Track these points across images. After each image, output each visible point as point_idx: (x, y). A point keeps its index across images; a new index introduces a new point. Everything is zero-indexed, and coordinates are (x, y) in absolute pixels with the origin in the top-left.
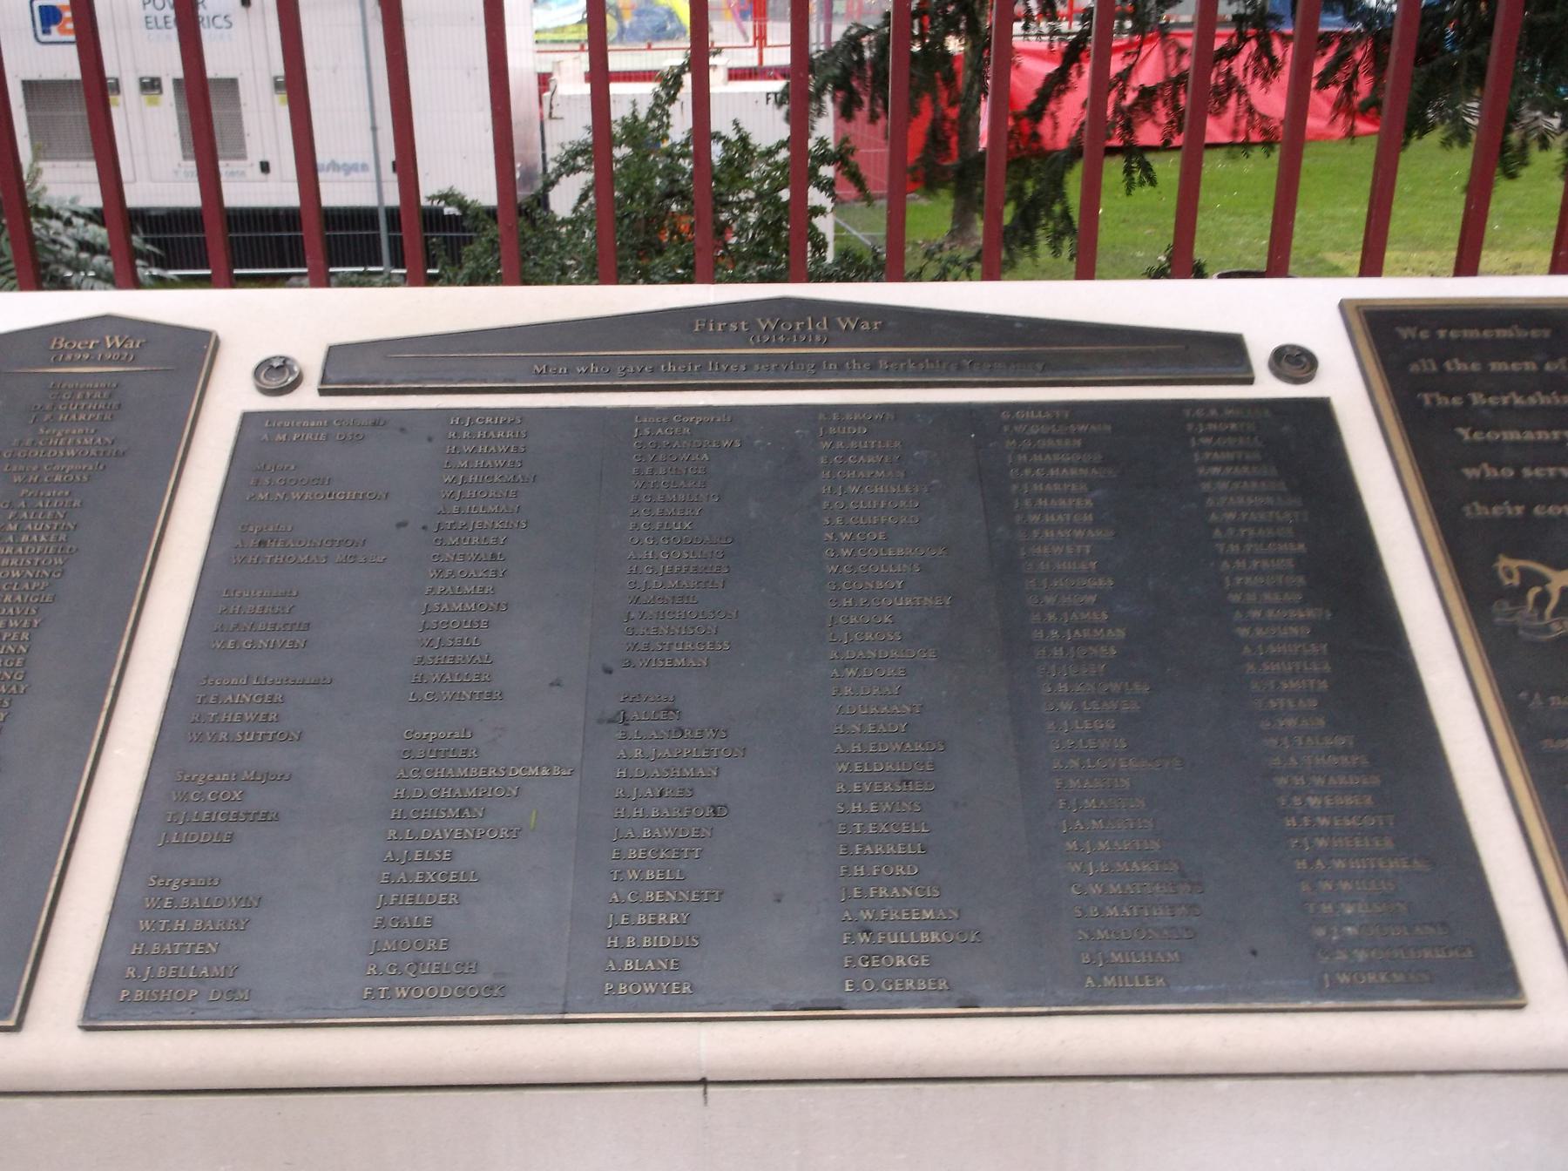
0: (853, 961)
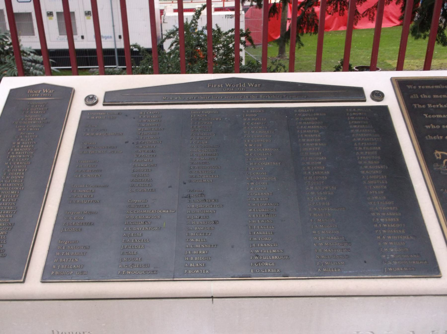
0: (253, 264)
